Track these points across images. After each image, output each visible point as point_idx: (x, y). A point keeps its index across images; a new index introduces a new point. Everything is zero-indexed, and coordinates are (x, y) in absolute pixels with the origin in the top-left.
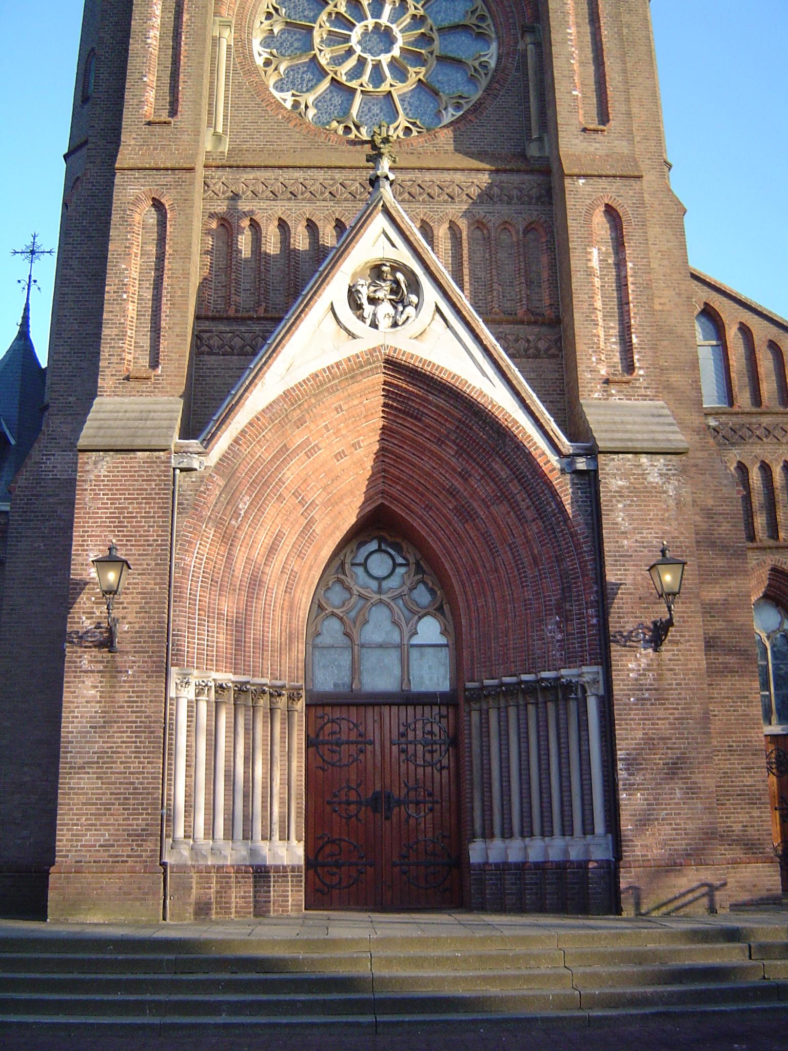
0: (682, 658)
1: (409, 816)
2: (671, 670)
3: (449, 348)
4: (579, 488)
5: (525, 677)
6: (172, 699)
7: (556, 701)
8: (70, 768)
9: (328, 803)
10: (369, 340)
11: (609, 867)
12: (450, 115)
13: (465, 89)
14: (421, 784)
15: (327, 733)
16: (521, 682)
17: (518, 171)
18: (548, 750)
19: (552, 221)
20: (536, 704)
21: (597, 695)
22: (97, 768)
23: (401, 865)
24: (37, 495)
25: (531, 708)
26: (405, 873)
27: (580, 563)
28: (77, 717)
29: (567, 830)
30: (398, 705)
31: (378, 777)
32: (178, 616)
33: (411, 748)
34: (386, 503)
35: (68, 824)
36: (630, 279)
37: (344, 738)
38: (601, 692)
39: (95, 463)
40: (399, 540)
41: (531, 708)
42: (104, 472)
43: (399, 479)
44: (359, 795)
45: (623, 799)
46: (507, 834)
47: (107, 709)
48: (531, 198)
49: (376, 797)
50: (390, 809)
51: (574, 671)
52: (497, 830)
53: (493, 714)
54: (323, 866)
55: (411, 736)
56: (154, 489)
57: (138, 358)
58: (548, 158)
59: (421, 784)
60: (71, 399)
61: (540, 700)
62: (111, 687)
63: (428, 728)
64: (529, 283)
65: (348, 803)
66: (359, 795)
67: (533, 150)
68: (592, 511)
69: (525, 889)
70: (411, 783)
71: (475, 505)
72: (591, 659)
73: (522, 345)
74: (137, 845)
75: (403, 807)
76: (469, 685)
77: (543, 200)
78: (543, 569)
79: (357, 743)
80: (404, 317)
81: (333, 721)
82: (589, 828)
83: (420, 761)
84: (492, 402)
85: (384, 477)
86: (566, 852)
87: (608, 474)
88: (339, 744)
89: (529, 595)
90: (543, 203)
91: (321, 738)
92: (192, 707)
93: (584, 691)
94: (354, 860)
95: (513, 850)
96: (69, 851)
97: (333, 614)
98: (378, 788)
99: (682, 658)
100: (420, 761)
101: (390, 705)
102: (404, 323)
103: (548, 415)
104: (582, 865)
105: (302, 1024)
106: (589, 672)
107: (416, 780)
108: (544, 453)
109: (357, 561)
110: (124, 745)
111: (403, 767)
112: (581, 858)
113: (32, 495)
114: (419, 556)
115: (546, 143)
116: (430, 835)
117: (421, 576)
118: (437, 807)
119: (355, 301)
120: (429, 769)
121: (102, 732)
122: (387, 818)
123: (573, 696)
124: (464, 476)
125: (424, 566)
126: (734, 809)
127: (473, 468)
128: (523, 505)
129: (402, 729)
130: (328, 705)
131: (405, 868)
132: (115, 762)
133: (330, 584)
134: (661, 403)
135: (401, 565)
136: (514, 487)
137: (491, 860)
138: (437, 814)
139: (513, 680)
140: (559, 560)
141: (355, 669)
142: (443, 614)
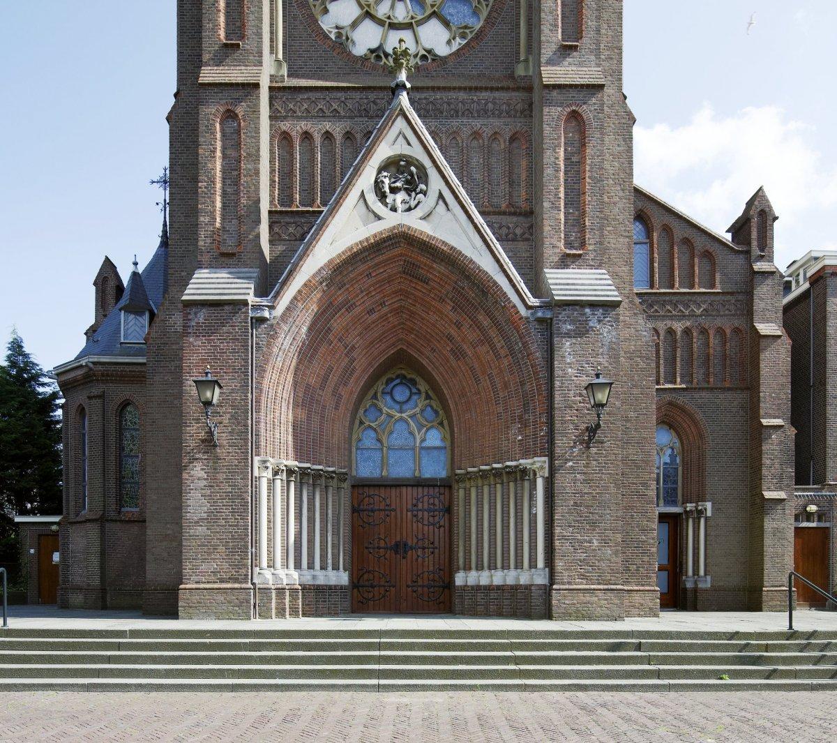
0: (604, 452)
1: (418, 556)
3: (450, 223)
4: (539, 332)
5: (495, 466)
6: (256, 478)
7: (516, 480)
8: (190, 522)
9: (366, 548)
10: (390, 221)
11: (545, 589)
12: (457, 43)
13: (471, 21)
14: (426, 536)
15: (365, 504)
16: (493, 469)
17: (507, 89)
18: (509, 514)
19: (531, 131)
20: (502, 483)
21: (543, 477)
22: (207, 522)
23: (413, 586)
24: (164, 344)
25: (499, 486)
26: (415, 592)
27: (537, 386)
28: (193, 489)
29: (518, 565)
30: (412, 486)
31: (398, 532)
33: (420, 514)
34: (405, 348)
35: (190, 559)
36: (588, 174)
37: (376, 508)
38: (546, 475)
39: (196, 314)
40: (413, 376)
41: (499, 486)
42: (201, 320)
43: (412, 329)
44: (386, 543)
45: (557, 546)
46: (480, 568)
47: (212, 484)
48: (516, 111)
49: (397, 545)
50: (406, 552)
51: (529, 461)
52: (473, 565)
53: (473, 491)
54: (363, 586)
55: (420, 506)
56: (238, 332)
57: (226, 240)
58: (531, 76)
59: (426, 536)
60: (183, 274)
61: (505, 481)
62: (215, 469)
63: (431, 501)
64: (511, 183)
65: (379, 548)
66: (386, 543)
67: (520, 71)
68: (547, 348)
69: (490, 602)
70: (420, 536)
71: (465, 347)
72: (541, 452)
73: (504, 231)
74: (236, 572)
75: (414, 550)
76: (458, 472)
77: (525, 113)
78: (511, 391)
79: (384, 510)
80: (416, 202)
81: (369, 496)
82: (533, 565)
83: (426, 522)
85: (403, 328)
86: (518, 579)
87: (561, 321)
88: (373, 511)
89: (500, 409)
90: (525, 117)
91: (362, 507)
92: (271, 483)
93: (535, 474)
94: (382, 583)
95: (484, 578)
96: (191, 575)
97: (370, 427)
98: (398, 539)
99: (604, 452)
100: (426, 522)
101: (407, 486)
102: (416, 207)
103: (519, 278)
104: (528, 588)
105: (182, 685)
106: (539, 463)
107: (423, 534)
108: (514, 306)
109: (386, 391)
110: (224, 507)
111: (415, 525)
112: (528, 583)
113: (161, 343)
114: (427, 387)
115: (531, 64)
116: (431, 568)
117: (428, 401)
118: (437, 551)
119: (380, 190)
120: (431, 527)
121: (209, 499)
122: (404, 558)
123: (527, 478)
124: (458, 325)
125: (431, 395)
127: (465, 319)
128: (498, 346)
129: (415, 502)
130: (366, 486)
131: (415, 589)
132: (219, 519)
133: (368, 406)
134: (604, 271)
135: (415, 393)
136: (493, 333)
137: (469, 584)
138: (437, 555)
139: (487, 468)
140: (522, 384)
141: (384, 463)
142: (443, 427)
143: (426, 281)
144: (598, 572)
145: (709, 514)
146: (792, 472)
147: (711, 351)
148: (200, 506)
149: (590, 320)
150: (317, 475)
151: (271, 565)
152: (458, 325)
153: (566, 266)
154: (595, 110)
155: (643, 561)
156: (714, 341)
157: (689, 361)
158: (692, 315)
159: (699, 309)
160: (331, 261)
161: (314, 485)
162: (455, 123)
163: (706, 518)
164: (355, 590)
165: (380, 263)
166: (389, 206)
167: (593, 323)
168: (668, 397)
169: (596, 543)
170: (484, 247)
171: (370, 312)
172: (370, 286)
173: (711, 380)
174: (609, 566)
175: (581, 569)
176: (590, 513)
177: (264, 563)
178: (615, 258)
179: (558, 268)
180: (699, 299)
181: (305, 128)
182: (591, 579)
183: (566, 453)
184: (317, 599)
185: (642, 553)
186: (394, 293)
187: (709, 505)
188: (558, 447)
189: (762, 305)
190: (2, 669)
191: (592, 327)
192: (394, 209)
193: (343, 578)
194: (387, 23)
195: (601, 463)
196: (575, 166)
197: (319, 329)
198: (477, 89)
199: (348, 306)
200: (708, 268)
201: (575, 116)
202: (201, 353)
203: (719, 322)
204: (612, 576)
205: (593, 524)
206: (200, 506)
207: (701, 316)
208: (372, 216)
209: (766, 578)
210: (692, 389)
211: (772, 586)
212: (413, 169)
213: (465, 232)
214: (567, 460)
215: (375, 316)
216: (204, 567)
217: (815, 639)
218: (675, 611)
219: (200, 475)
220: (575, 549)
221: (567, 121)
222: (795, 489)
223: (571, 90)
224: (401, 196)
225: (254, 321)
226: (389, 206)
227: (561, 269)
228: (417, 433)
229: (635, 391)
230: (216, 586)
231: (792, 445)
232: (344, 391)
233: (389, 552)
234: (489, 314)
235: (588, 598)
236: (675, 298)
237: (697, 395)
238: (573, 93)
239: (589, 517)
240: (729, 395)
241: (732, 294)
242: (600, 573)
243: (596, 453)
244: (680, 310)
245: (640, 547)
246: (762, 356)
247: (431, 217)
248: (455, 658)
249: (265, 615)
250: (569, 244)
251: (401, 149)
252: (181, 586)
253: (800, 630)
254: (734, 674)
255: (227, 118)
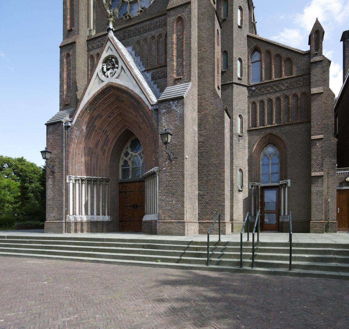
2: (174, 166)
32: (68, 163)
54: (123, 221)
79: (130, 192)
84: (135, 93)
88: (126, 192)
92: (74, 185)
99: (178, 162)
108: (147, 106)
124: (137, 116)
126: (214, 207)
132: (55, 198)
143: (123, 102)
144: (175, 215)
145: (289, 185)
146: (335, 161)
147: (290, 106)
148: (50, 194)
149: (172, 106)
150: (95, 181)
151: (74, 213)
152: (137, 116)
153: (176, 84)
154: (188, 13)
155: (219, 209)
156: (291, 101)
157: (279, 113)
158: (281, 90)
159: (284, 87)
160: (88, 101)
161: (94, 184)
162: (145, 35)
163: (289, 188)
164: (120, 223)
165: (107, 98)
166: (106, 76)
167: (174, 108)
168: (268, 131)
169: (174, 202)
170: (137, 84)
171: (109, 117)
172: (106, 108)
173: (290, 120)
174: (180, 212)
175: (168, 213)
176: (172, 189)
177: (71, 213)
178: (207, 75)
179: (173, 86)
180: (284, 82)
181: (98, 52)
182: (172, 218)
183: (163, 164)
184: (94, 226)
185: (218, 205)
186: (116, 108)
187: (289, 181)
188: (160, 162)
189: (316, 78)
190: (1, 249)
191: (173, 109)
192: (108, 77)
193: (107, 218)
194: (129, 3)
195: (176, 167)
196: (180, 40)
197: (91, 127)
198: (153, 18)
199: (100, 116)
200: (289, 66)
201: (180, 19)
202: (51, 141)
203: (294, 91)
204: (181, 216)
205: (173, 194)
206: (50, 194)
207: (285, 90)
208: (101, 81)
209: (312, 216)
210: (280, 126)
211: (316, 220)
212: (113, 60)
213: (130, 80)
214: (163, 167)
215: (112, 118)
216: (51, 215)
217: (228, 246)
218: (278, 232)
219: (50, 183)
220: (166, 205)
221: (177, 22)
222: (337, 170)
223: (178, 8)
224: (108, 73)
225: (66, 127)
226: (106, 76)
227: (174, 85)
228: (141, 161)
229: (216, 133)
230: (54, 221)
231: (335, 147)
232: (105, 148)
233: (131, 208)
234: (142, 111)
235: (170, 226)
236: (271, 84)
237: (282, 129)
238: (179, 9)
239: (172, 191)
240: (300, 126)
241: (301, 76)
242: (176, 215)
243: (174, 163)
244: (274, 89)
245: (218, 203)
246: (312, 105)
247: (120, 77)
248: (75, 248)
249: (69, 231)
250: (178, 74)
251: (110, 53)
252: (311, 222)
253: (194, 241)
254: (163, 260)
255: (68, 56)
